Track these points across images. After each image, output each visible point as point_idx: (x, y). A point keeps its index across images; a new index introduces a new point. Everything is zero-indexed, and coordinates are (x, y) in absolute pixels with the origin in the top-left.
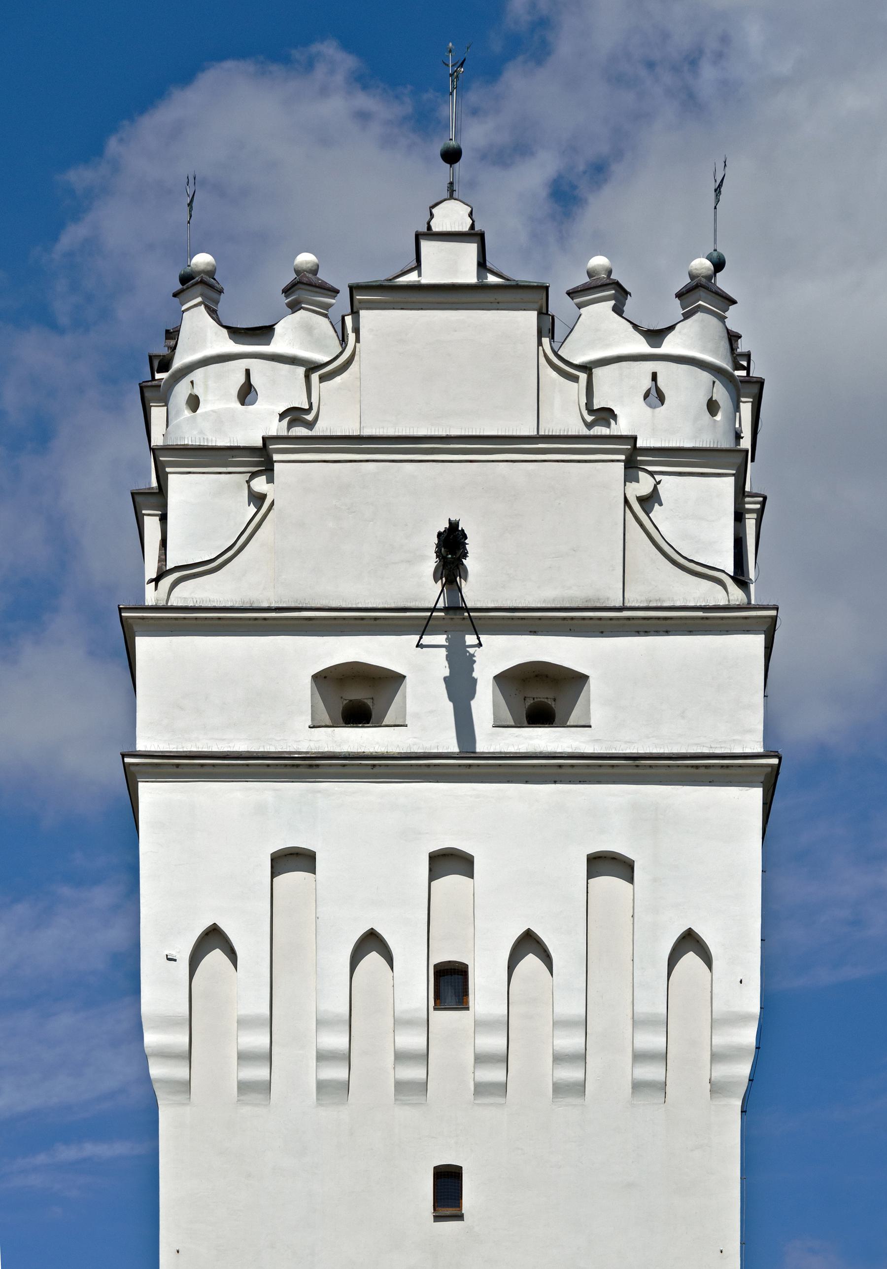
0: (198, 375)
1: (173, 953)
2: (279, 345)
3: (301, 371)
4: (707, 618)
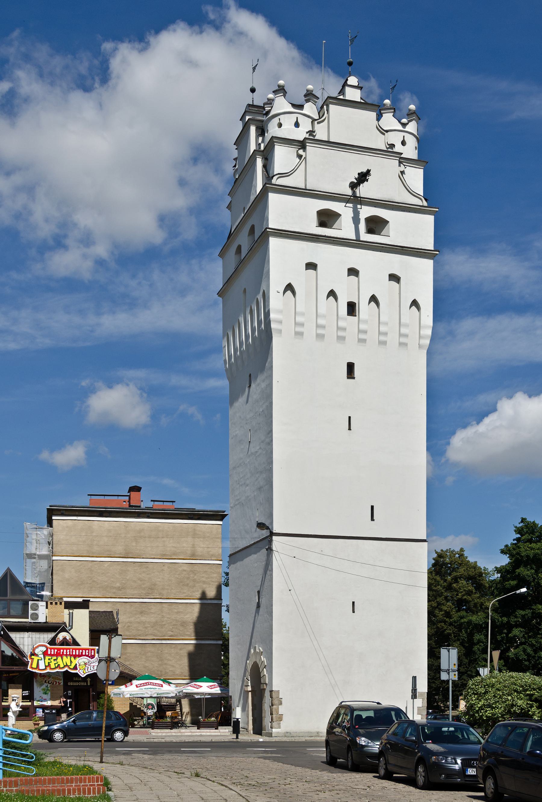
0: (281, 117)
1: (279, 291)
2: (304, 111)
3: (310, 120)
4: (420, 209)
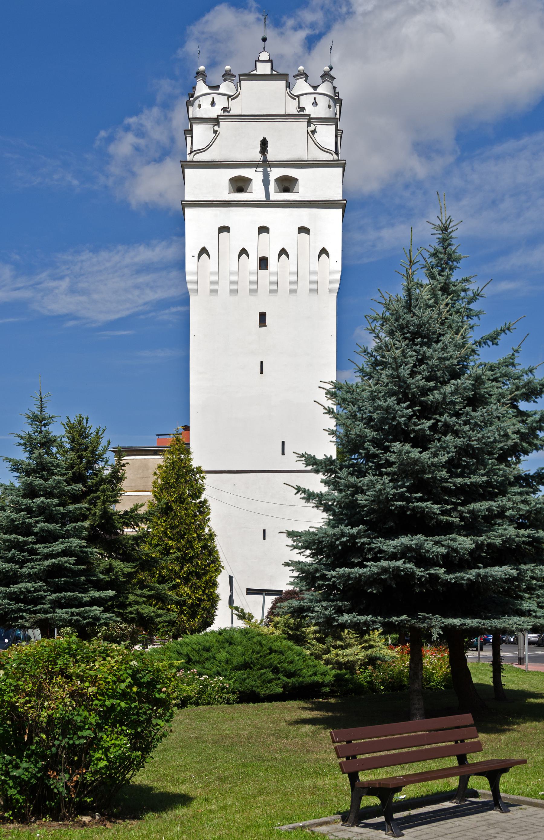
0: (201, 99)
2: (221, 91)
3: (226, 97)
